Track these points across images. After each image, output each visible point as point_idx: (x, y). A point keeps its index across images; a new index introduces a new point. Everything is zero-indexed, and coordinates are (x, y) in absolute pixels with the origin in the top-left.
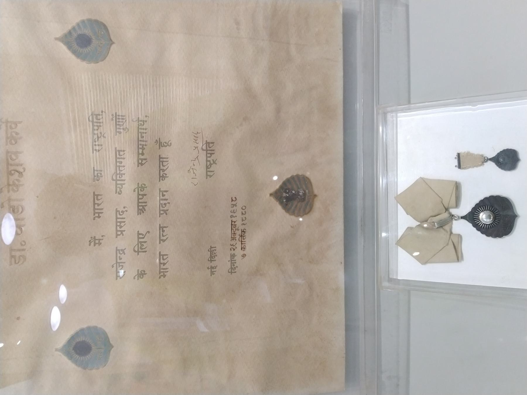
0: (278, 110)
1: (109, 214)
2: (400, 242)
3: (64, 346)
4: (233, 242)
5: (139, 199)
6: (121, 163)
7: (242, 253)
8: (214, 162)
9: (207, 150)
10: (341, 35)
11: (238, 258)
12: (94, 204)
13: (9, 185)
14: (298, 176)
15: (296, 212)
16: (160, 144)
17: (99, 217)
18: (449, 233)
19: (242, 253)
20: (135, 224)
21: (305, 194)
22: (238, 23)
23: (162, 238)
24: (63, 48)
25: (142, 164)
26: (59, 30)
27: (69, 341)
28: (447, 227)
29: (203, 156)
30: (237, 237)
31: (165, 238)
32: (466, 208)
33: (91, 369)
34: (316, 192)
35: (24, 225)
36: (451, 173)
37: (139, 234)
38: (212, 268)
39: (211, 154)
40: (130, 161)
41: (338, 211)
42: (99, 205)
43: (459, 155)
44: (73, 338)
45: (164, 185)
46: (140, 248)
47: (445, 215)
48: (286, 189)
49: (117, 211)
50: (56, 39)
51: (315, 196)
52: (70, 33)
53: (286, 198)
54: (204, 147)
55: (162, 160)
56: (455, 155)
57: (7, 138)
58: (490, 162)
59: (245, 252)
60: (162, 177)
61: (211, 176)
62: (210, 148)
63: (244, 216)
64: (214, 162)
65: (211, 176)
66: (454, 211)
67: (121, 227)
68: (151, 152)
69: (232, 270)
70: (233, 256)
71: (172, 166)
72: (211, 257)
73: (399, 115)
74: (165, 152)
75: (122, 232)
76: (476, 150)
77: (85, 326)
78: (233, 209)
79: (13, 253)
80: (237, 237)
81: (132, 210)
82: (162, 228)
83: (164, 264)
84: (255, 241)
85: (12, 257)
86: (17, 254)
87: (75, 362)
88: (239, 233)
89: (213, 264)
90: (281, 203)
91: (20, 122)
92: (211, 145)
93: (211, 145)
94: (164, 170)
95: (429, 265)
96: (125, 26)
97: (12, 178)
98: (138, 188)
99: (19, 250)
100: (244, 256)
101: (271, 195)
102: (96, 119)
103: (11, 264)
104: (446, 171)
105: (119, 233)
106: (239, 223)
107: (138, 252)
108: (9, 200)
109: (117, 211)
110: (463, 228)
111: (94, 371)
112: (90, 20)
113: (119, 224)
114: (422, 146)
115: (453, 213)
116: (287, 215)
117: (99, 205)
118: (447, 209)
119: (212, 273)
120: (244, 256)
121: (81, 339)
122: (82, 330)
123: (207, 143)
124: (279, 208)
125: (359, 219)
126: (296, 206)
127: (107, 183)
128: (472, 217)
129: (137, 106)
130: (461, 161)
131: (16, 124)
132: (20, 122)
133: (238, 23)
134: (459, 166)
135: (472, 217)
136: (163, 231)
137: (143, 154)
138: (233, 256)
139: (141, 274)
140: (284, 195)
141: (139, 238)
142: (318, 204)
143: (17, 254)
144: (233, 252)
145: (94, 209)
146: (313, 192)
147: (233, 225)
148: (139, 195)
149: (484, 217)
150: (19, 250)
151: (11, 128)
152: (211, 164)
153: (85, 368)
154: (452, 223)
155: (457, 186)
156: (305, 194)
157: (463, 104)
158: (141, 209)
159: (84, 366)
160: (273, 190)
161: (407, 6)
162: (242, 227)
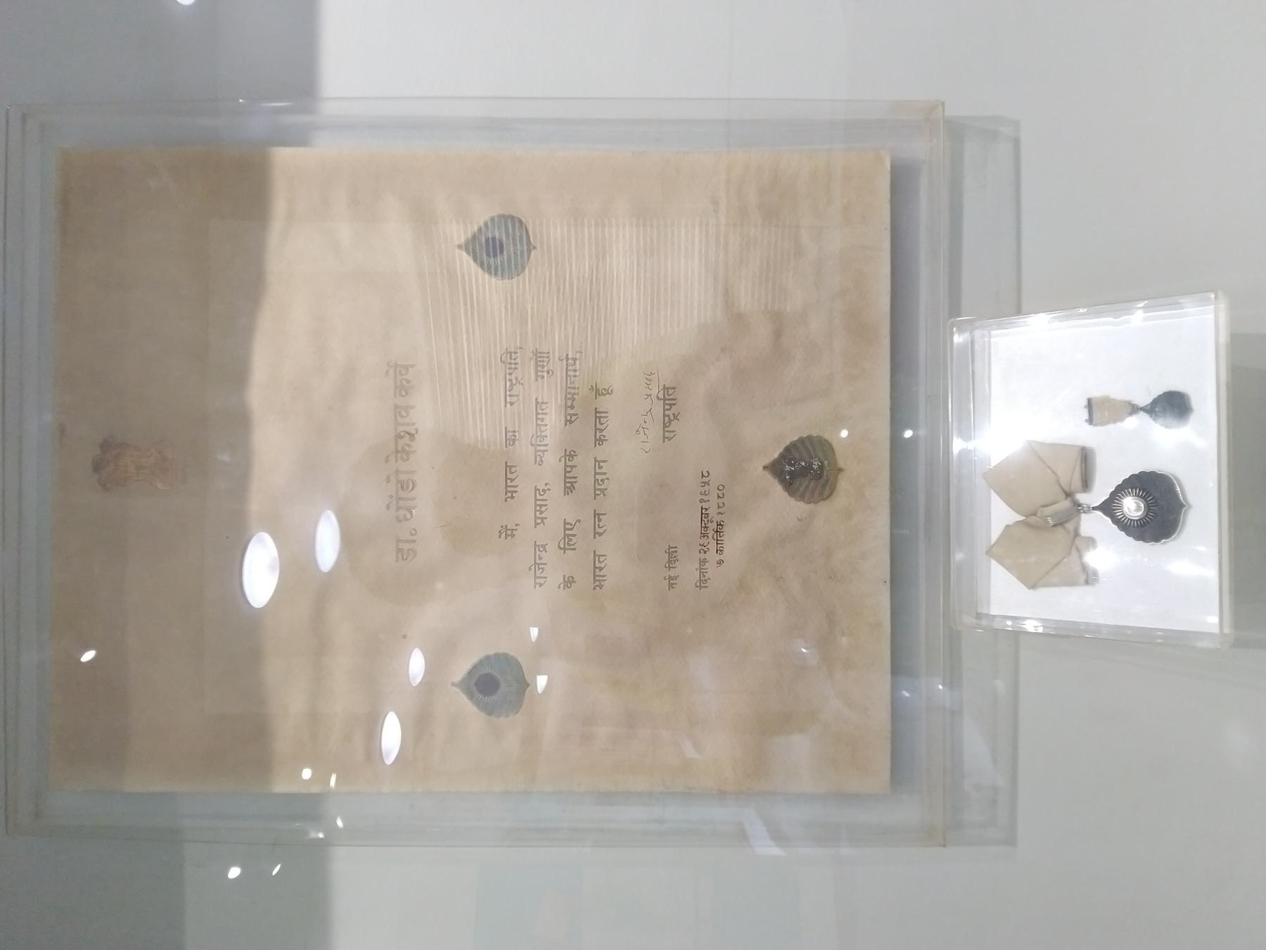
0: (778, 334)
1: (525, 491)
2: (990, 553)
3: (463, 681)
4: (704, 541)
5: (566, 472)
6: (543, 420)
7: (718, 557)
8: (675, 417)
9: (665, 400)
10: (887, 206)
11: (711, 568)
12: (507, 479)
13: (397, 452)
14: (810, 437)
15: (807, 496)
16: (597, 392)
17: (512, 497)
18: (1072, 535)
19: (718, 557)
20: (560, 509)
21: (821, 467)
22: (715, 203)
23: (598, 530)
24: (466, 259)
25: (571, 422)
26: (459, 233)
27: (470, 673)
28: (1070, 526)
29: (658, 409)
30: (711, 533)
31: (601, 530)
32: (1099, 494)
33: (498, 716)
34: (841, 463)
35: (414, 508)
36: (1076, 431)
37: (565, 523)
38: (671, 578)
39: (671, 405)
40: (554, 417)
41: (880, 494)
42: (512, 480)
43: (1089, 401)
44: (475, 667)
45: (601, 452)
46: (567, 542)
47: (1065, 504)
48: (790, 460)
49: (536, 489)
50: (460, 247)
51: (840, 470)
52: (474, 237)
53: (791, 473)
54: (661, 396)
55: (598, 415)
56: (1085, 403)
57: (396, 388)
58: (1142, 413)
59: (722, 557)
60: (600, 441)
61: (670, 439)
62: (669, 398)
63: (721, 501)
64: (675, 417)
65: (670, 439)
66: (1082, 498)
67: (541, 512)
68: (587, 412)
69: (702, 583)
70: (703, 562)
71: (613, 426)
72: (669, 562)
73: (993, 333)
74: (604, 403)
75: (542, 519)
76: (1118, 392)
77: (491, 653)
78: (703, 490)
79: (401, 546)
80: (711, 533)
81: (557, 488)
82: (597, 515)
83: (601, 569)
84: (737, 540)
85: (399, 550)
86: (406, 546)
87: (477, 704)
88: (713, 526)
89: (672, 573)
90: (782, 481)
91: (413, 366)
92: (671, 391)
93: (671, 391)
94: (601, 430)
95: (1043, 592)
96: (551, 229)
97: (401, 442)
98: (566, 455)
99: (408, 541)
100: (720, 562)
101: (765, 468)
102: (510, 359)
103: (397, 561)
104: (1071, 429)
105: (539, 521)
106: (712, 512)
107: (564, 549)
108: (397, 472)
109: (536, 489)
110: (1095, 524)
111: (502, 719)
112: (501, 216)
113: (539, 507)
114: (1035, 386)
115: (1081, 501)
116: (792, 501)
117: (512, 480)
118: (1069, 495)
119: (671, 586)
120: (720, 562)
121: (486, 670)
122: (488, 658)
123: (665, 388)
124: (777, 489)
125: (922, 510)
126: (807, 487)
127: (524, 450)
128: (1109, 508)
129: (566, 338)
130: (1097, 410)
131: (406, 368)
132: (413, 366)
133: (715, 203)
134: (1090, 421)
135: (1109, 508)
136: (600, 520)
137: (572, 407)
138: (703, 562)
139: (569, 582)
140: (788, 468)
141: (565, 529)
142: (843, 484)
143: (406, 546)
144: (703, 556)
145: (507, 486)
146: (836, 463)
147: (704, 514)
148: (566, 466)
149: (1132, 507)
150: (408, 541)
151: (401, 374)
152: (670, 421)
153: (490, 714)
154: (1079, 520)
155: (1085, 457)
156: (821, 467)
157: (1099, 314)
158: (569, 488)
159: (489, 710)
160: (767, 460)
161: (1016, 142)
162: (718, 518)
